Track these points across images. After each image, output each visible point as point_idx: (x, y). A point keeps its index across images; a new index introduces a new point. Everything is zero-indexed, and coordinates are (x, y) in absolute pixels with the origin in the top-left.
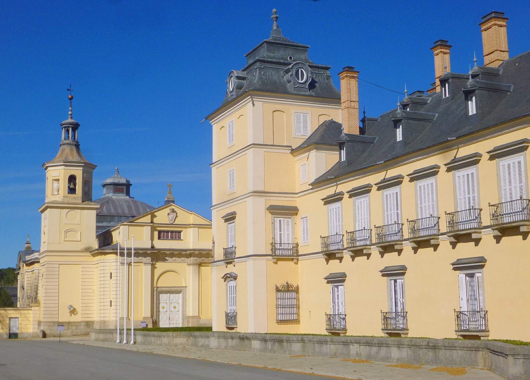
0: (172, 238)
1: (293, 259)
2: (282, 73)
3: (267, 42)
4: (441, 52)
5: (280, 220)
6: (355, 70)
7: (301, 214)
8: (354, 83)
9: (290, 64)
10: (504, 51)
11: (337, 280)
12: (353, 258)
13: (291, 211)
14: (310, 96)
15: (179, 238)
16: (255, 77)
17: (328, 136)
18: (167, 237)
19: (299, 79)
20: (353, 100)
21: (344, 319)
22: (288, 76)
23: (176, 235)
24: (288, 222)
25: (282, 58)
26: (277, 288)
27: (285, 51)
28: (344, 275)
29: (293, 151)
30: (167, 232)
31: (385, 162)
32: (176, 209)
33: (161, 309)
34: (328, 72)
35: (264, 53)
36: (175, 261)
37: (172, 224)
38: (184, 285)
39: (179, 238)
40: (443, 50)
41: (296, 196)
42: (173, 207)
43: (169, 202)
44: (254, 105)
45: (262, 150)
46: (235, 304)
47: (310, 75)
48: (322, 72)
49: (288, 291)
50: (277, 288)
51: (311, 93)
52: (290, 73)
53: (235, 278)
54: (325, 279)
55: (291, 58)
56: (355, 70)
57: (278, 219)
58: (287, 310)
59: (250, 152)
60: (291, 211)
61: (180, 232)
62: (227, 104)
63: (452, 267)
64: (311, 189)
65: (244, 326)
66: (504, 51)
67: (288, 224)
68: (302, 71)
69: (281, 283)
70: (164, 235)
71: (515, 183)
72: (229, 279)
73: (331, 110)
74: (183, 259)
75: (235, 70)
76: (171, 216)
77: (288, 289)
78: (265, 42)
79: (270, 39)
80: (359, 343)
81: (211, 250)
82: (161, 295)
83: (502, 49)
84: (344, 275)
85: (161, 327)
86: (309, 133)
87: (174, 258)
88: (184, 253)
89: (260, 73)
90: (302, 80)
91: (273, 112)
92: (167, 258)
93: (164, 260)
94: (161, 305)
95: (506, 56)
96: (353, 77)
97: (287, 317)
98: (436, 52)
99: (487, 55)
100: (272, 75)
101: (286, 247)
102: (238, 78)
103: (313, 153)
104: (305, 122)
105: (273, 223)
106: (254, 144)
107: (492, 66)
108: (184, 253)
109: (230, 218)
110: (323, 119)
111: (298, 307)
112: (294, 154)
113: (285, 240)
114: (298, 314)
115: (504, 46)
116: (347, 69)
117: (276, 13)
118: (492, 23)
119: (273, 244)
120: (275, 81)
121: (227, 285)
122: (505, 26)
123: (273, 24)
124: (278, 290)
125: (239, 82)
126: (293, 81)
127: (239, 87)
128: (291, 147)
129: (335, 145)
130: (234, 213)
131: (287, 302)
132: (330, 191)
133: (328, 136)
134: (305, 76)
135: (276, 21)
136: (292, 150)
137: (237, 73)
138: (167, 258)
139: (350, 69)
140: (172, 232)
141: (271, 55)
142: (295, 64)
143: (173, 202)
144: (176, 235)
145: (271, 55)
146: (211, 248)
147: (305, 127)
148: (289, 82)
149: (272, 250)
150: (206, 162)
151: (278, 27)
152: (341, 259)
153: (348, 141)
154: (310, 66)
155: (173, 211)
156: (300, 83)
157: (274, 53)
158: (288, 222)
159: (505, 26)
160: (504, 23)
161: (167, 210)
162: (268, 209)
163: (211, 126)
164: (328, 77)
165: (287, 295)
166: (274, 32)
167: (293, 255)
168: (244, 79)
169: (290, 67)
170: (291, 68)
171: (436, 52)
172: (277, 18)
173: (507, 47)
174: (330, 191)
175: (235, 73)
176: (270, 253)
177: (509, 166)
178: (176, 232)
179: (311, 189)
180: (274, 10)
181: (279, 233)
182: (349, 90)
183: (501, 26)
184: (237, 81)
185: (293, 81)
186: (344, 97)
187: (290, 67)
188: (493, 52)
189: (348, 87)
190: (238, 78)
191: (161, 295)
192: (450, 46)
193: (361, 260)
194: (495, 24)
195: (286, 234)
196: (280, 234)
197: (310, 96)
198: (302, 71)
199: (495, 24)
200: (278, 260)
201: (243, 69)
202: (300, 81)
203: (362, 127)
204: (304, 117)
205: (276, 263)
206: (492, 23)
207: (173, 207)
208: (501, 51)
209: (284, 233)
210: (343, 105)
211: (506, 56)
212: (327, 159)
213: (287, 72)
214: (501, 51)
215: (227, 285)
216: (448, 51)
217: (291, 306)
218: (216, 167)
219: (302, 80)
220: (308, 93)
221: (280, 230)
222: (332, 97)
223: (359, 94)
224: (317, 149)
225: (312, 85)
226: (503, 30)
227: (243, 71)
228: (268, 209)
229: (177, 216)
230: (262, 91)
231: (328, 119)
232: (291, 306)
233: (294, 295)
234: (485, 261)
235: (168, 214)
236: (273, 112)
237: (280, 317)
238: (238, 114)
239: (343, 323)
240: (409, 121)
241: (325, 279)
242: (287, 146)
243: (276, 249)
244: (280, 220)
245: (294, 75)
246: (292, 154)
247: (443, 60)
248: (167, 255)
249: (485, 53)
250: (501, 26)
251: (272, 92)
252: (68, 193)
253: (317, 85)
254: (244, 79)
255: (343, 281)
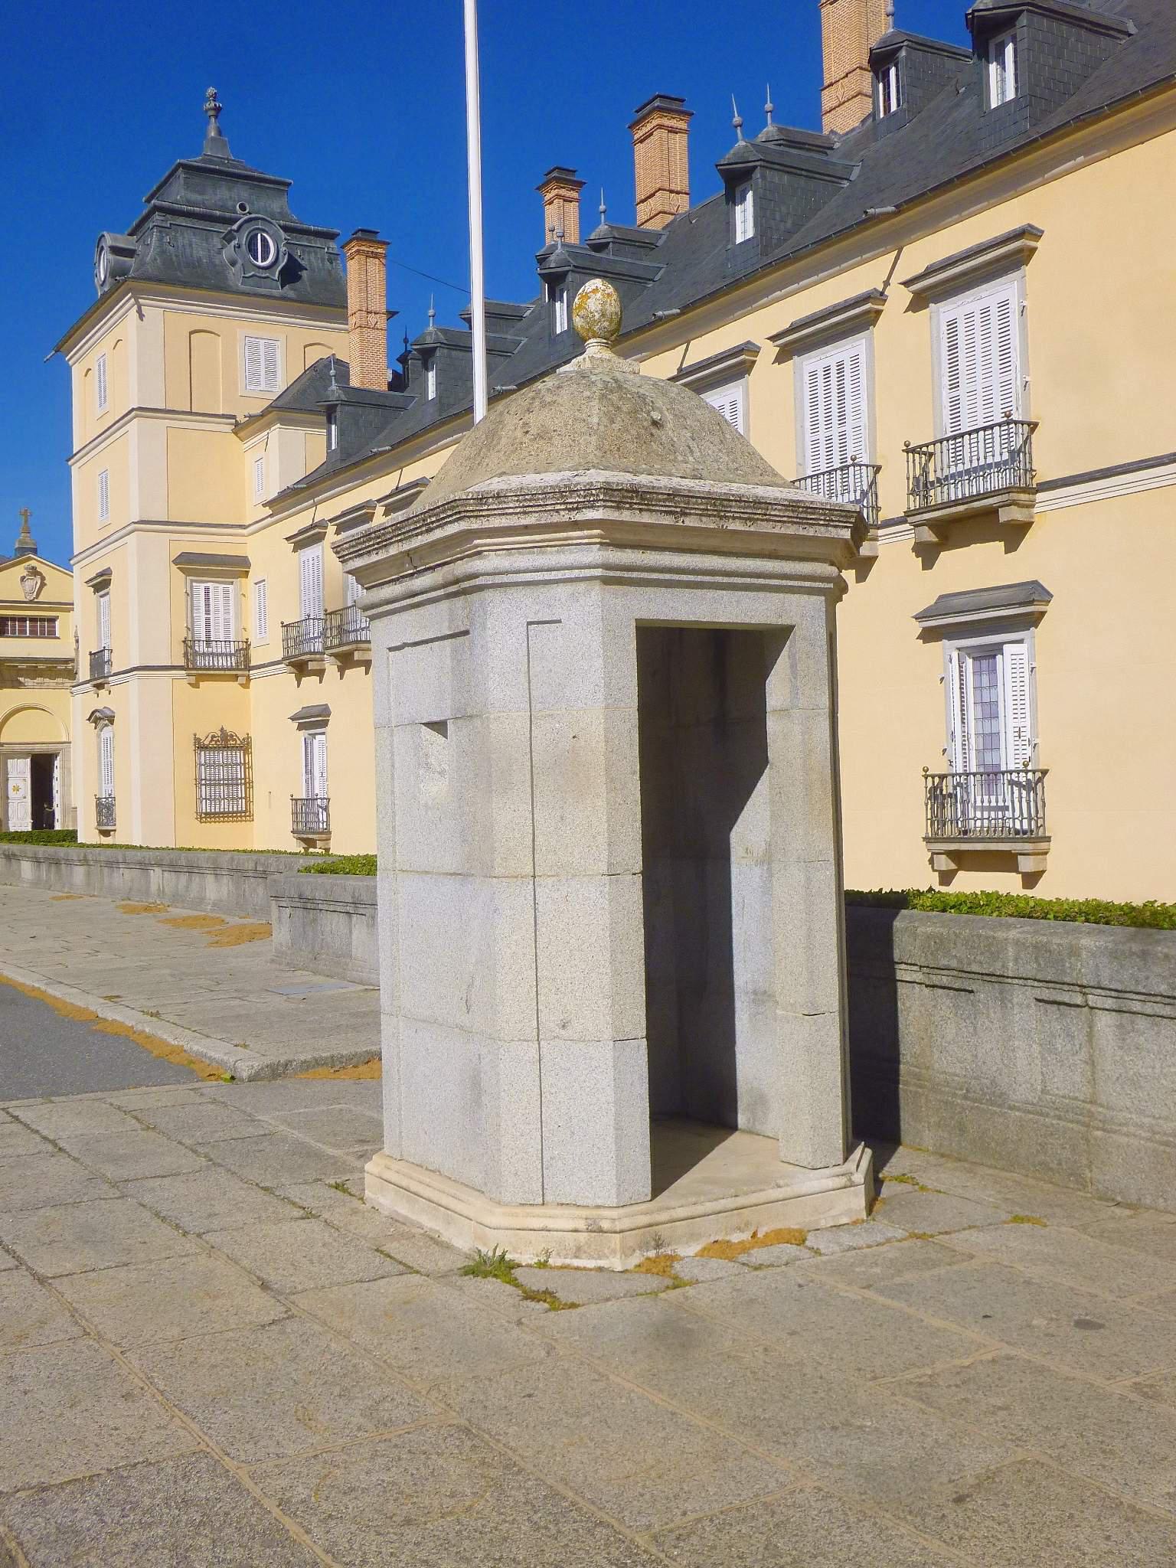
0: (34, 634)
1: (237, 676)
2: (216, 242)
3: (187, 167)
4: (558, 196)
5: (207, 590)
6: (379, 238)
7: (255, 573)
8: (376, 271)
9: (233, 221)
10: (678, 193)
11: (313, 720)
12: (342, 671)
13: (235, 567)
14: (284, 298)
15: (52, 634)
16: (150, 248)
17: (317, 397)
18: (23, 632)
19: (256, 259)
20: (373, 309)
21: (326, 809)
22: (229, 251)
23: (44, 626)
24: (226, 592)
25: (222, 208)
26: (197, 740)
27: (230, 190)
28: (325, 711)
29: (239, 429)
30: (23, 619)
31: (394, 447)
32: (41, 568)
33: (11, 793)
34: (333, 245)
35: (179, 194)
36: (41, 686)
37: (31, 602)
38: (64, 739)
39: (52, 634)
40: (562, 192)
41: (245, 532)
42: (33, 563)
43: (24, 552)
44: (141, 316)
45: (161, 424)
46: (110, 780)
47: (283, 249)
48: (318, 243)
49: (226, 747)
50: (197, 740)
51: (288, 291)
52: (235, 242)
53: (111, 720)
54: (293, 719)
55: (243, 208)
56: (379, 238)
57: (203, 586)
58: (222, 790)
59: (134, 426)
60: (235, 567)
61: (52, 620)
62: (91, 312)
63: (917, 628)
64: (271, 516)
65: (130, 831)
66: (678, 193)
67: (226, 598)
68: (264, 240)
69: (207, 729)
70: (14, 627)
71: (972, 379)
72: (102, 722)
73: (334, 334)
74: (60, 680)
75: (109, 231)
76: (29, 583)
77: (227, 743)
78: (180, 165)
79: (195, 161)
80: (160, 865)
81: (72, 660)
82: (10, 762)
83: (673, 187)
84: (325, 711)
85: (12, 829)
86: (280, 386)
87: (39, 680)
88: (61, 667)
89: (160, 239)
90: (264, 259)
91: (191, 333)
92: (21, 679)
93: (18, 685)
94: (11, 784)
95: (683, 203)
96: (375, 256)
97: (224, 806)
98: (548, 196)
99: (643, 201)
100: (191, 245)
101: (220, 648)
102: (115, 250)
103: (276, 432)
104: (271, 362)
105: (190, 595)
106: (140, 409)
107: (648, 226)
108: (61, 667)
109: (101, 583)
110: (315, 355)
111: (248, 784)
112: (241, 434)
113: (218, 634)
114: (248, 800)
115: (681, 179)
116: (359, 234)
117: (215, 97)
118: (655, 123)
119: (189, 644)
120: (199, 260)
121: (99, 736)
122: (686, 131)
123: (208, 123)
124: (200, 747)
125: (116, 262)
126: (240, 262)
127: (118, 274)
128: (234, 417)
129: (318, 413)
130: (107, 572)
131: (222, 773)
132: (301, 520)
133: (317, 397)
134: (273, 249)
135: (216, 117)
136: (237, 424)
137: (115, 239)
138: (21, 679)
139: (367, 235)
140: (33, 620)
141: (195, 197)
142: (246, 221)
143: (35, 551)
144: (44, 626)
145: (195, 197)
146: (72, 655)
147: (271, 373)
148: (233, 263)
149: (186, 654)
150: (64, 454)
151: (220, 132)
152: (320, 673)
153: (344, 403)
154: (285, 229)
155: (34, 572)
156: (259, 267)
157: (201, 193)
158: (226, 592)
159: (686, 131)
160: (683, 125)
161: (20, 570)
162: (175, 562)
163: (70, 368)
164: (333, 257)
165: (220, 757)
166: (212, 144)
167: (241, 667)
168: (130, 253)
169: (235, 227)
170: (238, 231)
171: (548, 196)
172: (218, 110)
173: (686, 182)
174: (301, 520)
175: (109, 240)
176: (182, 662)
177: (952, 325)
178: (42, 620)
179: (271, 516)
180: (211, 90)
181: (204, 616)
182: (363, 286)
183: (673, 131)
184: (111, 257)
185: (240, 262)
186: (353, 303)
187: (235, 227)
188: (652, 195)
189: (364, 279)
190: (115, 250)
191: (10, 762)
192: (580, 184)
193: (355, 674)
194: (660, 126)
195: (221, 621)
196: (207, 619)
197: (284, 298)
198: (264, 240)
199: (660, 126)
200: (201, 678)
201: (130, 230)
202: (259, 263)
203: (400, 371)
204: (273, 348)
205: (196, 685)
206: (655, 123)
207: (33, 563)
208: (671, 192)
209: (218, 618)
210: (352, 320)
211: (683, 203)
212: (305, 447)
213: (228, 238)
214: (671, 192)
215: (99, 736)
216: (575, 195)
217: (232, 782)
218: (79, 464)
219: (264, 259)
220: (278, 292)
221: (207, 612)
222: (327, 302)
223: (387, 296)
224: (284, 422)
225: (291, 273)
226: (680, 142)
227: (131, 234)
228: (175, 562)
229: (43, 585)
230: (160, 281)
231: (325, 354)
232: (232, 782)
233: (239, 756)
234: (1046, 596)
235: (23, 579)
236: (191, 333)
237: (206, 807)
238: (110, 340)
239: (323, 816)
240: (454, 353)
241: (293, 719)
242: (223, 416)
243: (196, 653)
244: (207, 590)
245: (244, 247)
246: (236, 434)
247: (563, 217)
248: (21, 672)
249: (639, 197)
250: (673, 131)
251: (185, 284)
252: (344, 320)
253: (304, 274)
254: (130, 253)
255: (325, 724)
